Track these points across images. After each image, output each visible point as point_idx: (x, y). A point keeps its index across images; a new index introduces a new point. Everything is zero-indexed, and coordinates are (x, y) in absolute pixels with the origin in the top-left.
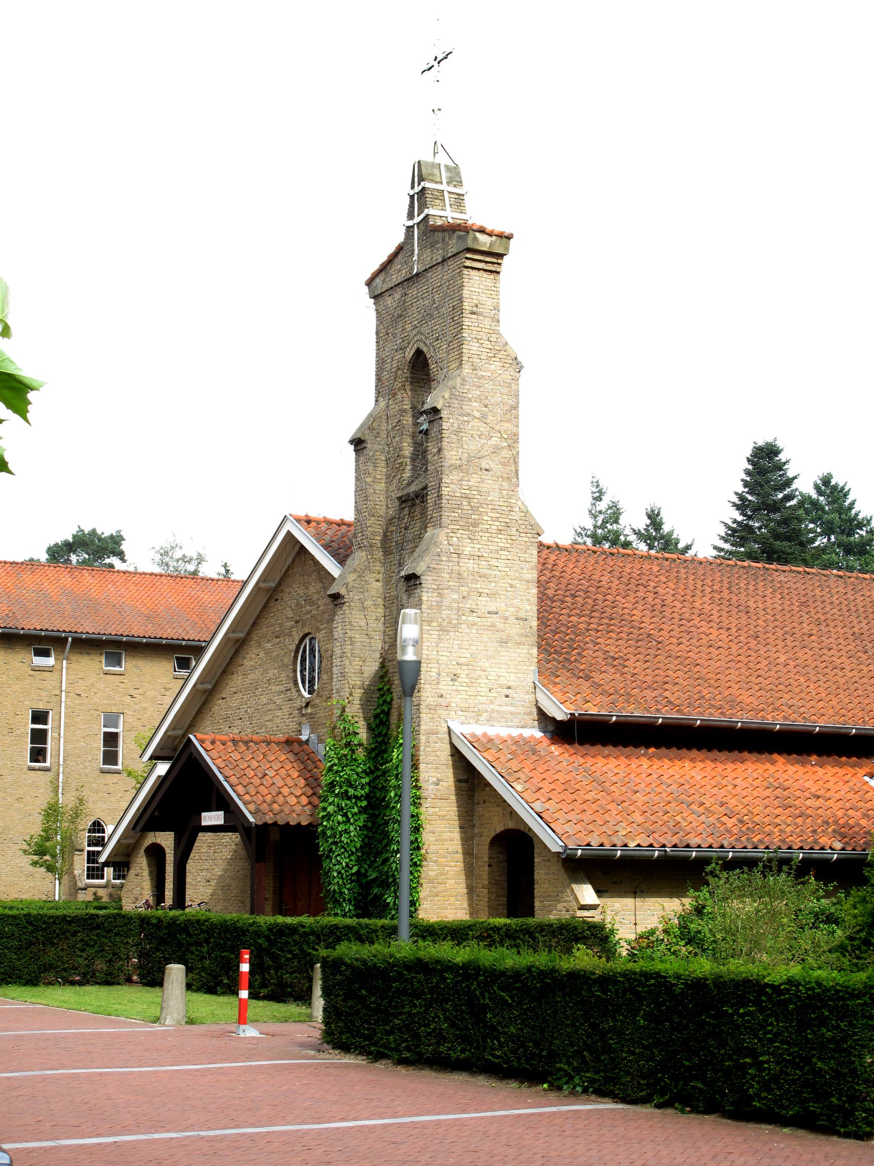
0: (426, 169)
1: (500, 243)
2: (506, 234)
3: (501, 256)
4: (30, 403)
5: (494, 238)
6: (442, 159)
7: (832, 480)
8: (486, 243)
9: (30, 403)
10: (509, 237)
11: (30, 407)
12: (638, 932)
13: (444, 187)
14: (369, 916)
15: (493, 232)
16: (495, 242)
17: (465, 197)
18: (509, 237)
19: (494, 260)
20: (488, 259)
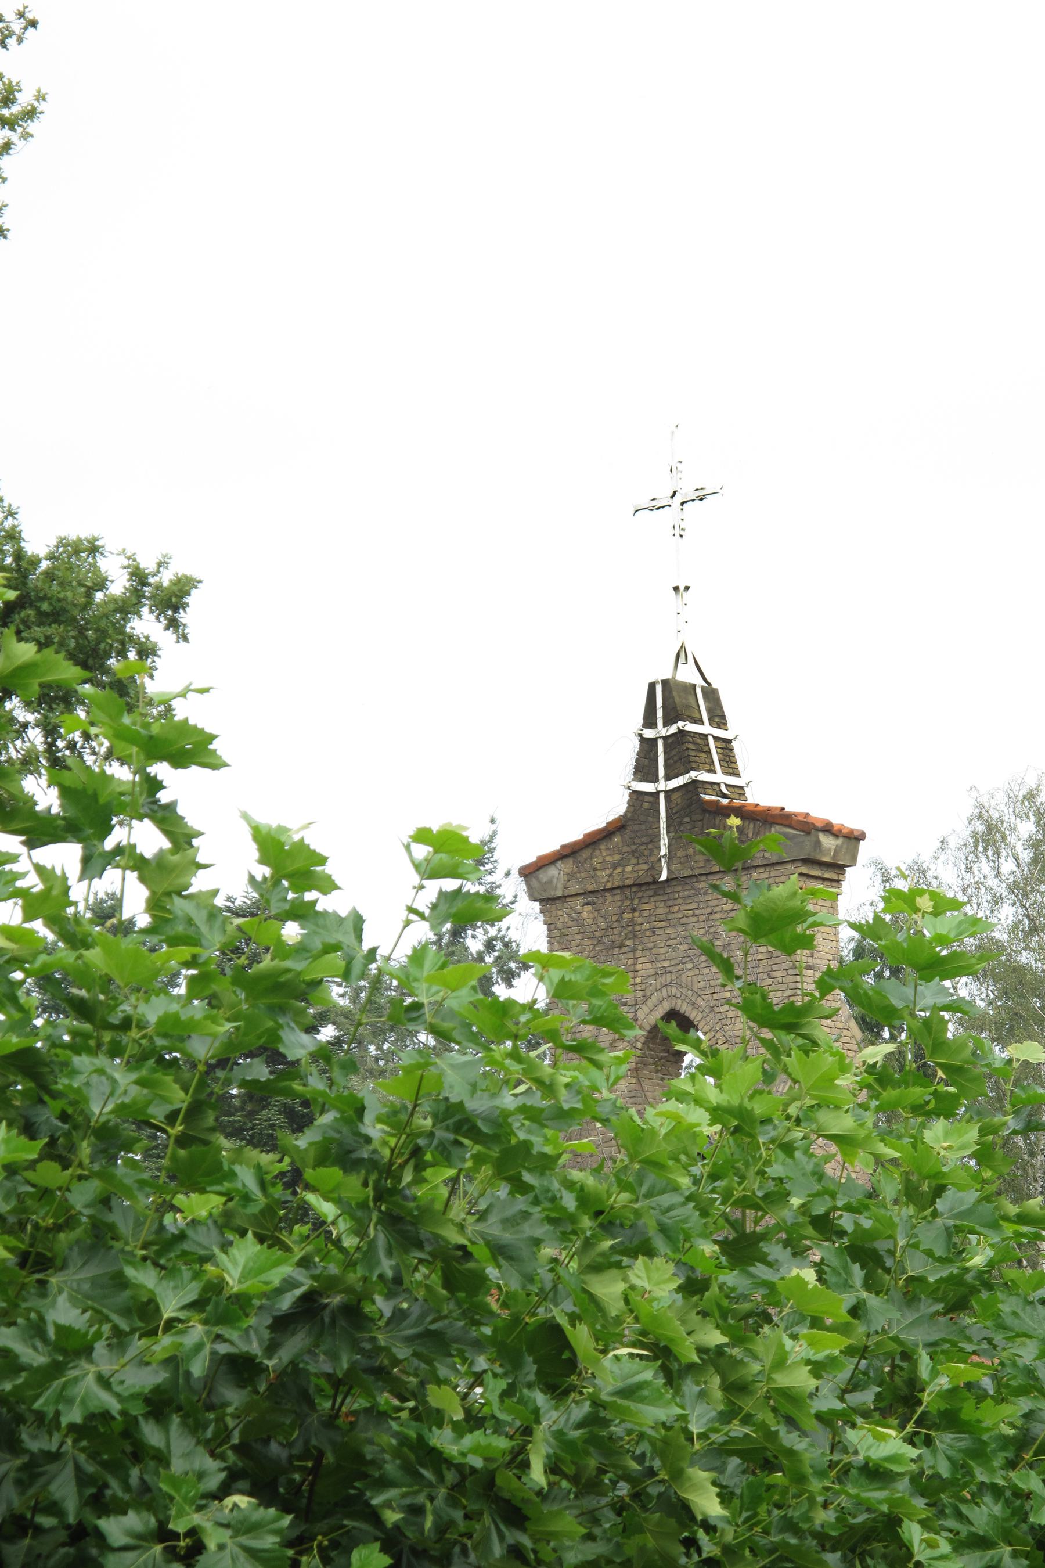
0: (680, 697)
1: (847, 849)
2: (856, 834)
3: (840, 868)
4: (186, 720)
5: (840, 841)
6: (687, 675)
7: (942, 1408)
8: (830, 849)
9: (186, 720)
10: (860, 837)
11: (191, 722)
12: (127, 829)
13: (706, 729)
14: (1020, 1480)
15: (840, 831)
16: (841, 847)
17: (734, 743)
18: (860, 837)
19: (827, 875)
20: (827, 875)
